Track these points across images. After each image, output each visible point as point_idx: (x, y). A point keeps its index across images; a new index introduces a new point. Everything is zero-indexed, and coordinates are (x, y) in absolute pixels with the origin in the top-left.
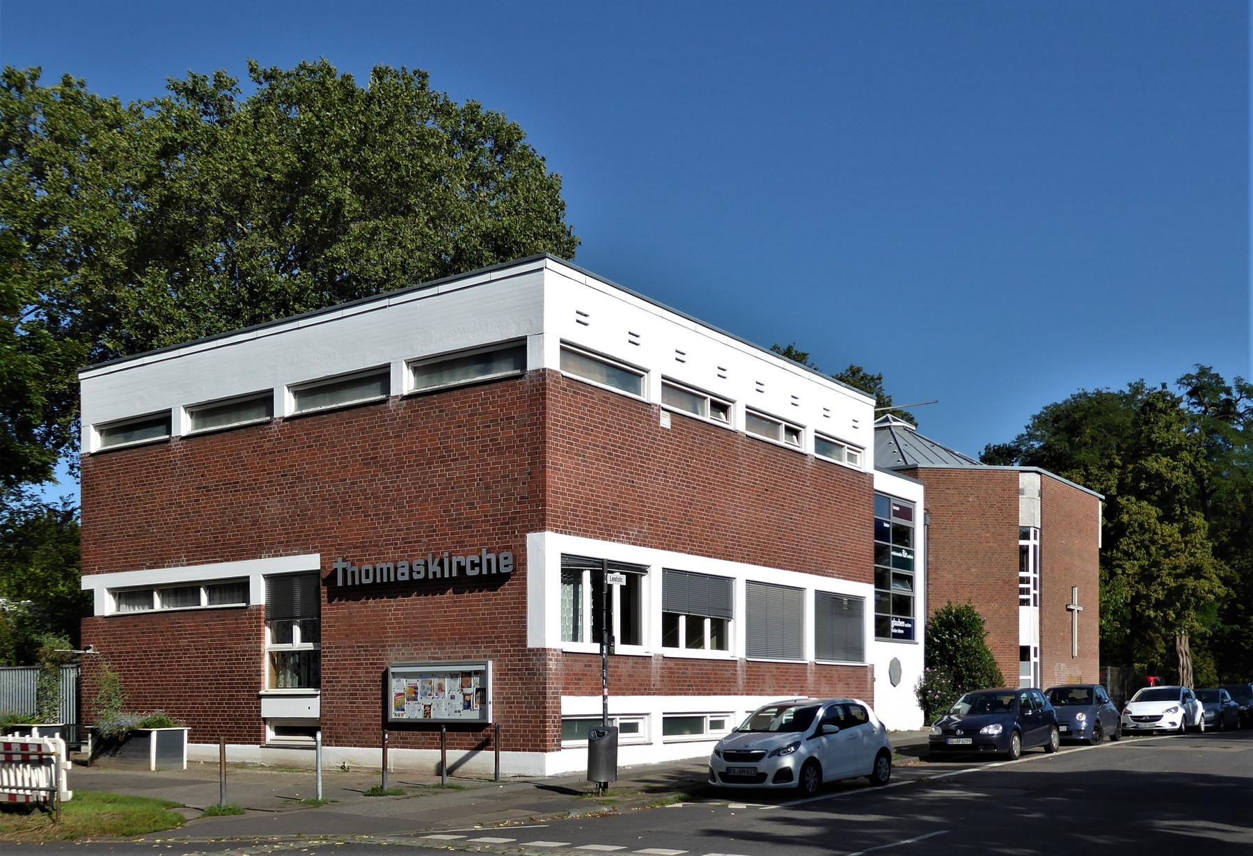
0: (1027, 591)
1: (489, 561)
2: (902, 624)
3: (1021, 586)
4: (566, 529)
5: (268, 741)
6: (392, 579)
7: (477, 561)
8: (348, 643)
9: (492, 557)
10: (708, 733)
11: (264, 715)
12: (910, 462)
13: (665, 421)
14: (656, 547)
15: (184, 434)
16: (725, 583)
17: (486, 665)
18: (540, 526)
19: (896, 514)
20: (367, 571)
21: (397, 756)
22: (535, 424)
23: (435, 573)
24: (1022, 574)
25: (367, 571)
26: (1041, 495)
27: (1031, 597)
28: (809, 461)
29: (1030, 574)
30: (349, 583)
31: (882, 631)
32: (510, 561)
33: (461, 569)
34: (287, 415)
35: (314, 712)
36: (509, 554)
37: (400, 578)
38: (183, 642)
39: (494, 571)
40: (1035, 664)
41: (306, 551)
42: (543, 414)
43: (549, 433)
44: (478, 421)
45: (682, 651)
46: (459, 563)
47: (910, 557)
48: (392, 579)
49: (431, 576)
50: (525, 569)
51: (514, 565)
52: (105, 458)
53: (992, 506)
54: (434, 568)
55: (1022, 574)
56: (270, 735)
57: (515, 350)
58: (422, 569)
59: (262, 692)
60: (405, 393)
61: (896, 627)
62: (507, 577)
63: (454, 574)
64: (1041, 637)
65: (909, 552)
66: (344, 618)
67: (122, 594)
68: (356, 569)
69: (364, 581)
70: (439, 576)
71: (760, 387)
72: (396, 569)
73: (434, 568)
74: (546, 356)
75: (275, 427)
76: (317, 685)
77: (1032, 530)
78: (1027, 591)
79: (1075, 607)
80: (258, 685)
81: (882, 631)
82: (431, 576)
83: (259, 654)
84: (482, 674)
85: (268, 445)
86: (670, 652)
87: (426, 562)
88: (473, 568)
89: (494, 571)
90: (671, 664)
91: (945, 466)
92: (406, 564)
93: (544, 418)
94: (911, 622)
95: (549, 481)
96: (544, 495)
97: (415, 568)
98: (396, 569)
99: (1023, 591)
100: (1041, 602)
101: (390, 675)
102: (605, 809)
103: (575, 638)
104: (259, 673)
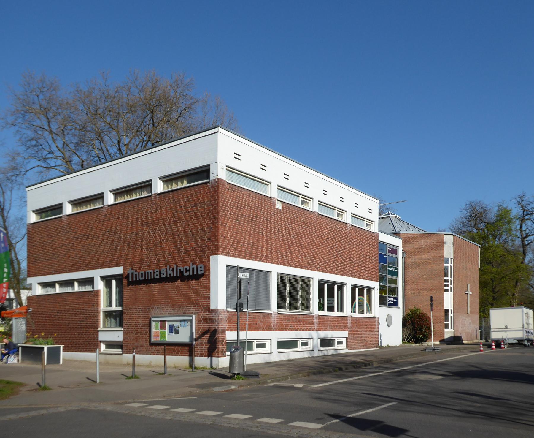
0: (447, 286)
1: (193, 268)
2: (392, 299)
3: (445, 283)
4: (229, 254)
5: (102, 351)
6: (152, 277)
7: (188, 269)
8: (134, 307)
9: (195, 266)
10: (300, 348)
11: (100, 339)
12: (398, 231)
13: (279, 206)
14: (274, 263)
15: (68, 214)
16: (267, 273)
17: (192, 317)
18: (216, 252)
19: (389, 251)
20: (142, 274)
21: (141, 358)
22: (214, 205)
23: (170, 275)
24: (445, 278)
25: (142, 274)
26: (454, 244)
27: (449, 288)
28: (348, 227)
29: (449, 278)
30: (134, 280)
31: (383, 302)
32: (202, 269)
33: (181, 272)
34: (110, 204)
35: (121, 339)
36: (202, 265)
37: (156, 277)
38: (67, 307)
39: (195, 273)
40: (451, 317)
41: (117, 265)
42: (217, 200)
43: (220, 209)
44: (189, 204)
45: (357, 315)
46: (180, 270)
47: (396, 270)
48: (152, 277)
49: (168, 276)
50: (209, 272)
51: (204, 270)
52: (36, 225)
53: (432, 249)
54: (170, 272)
55: (445, 278)
56: (103, 347)
57: (204, 172)
58: (165, 273)
59: (99, 329)
60: (159, 192)
61: (390, 301)
62: (202, 275)
63: (178, 275)
64: (454, 305)
65: (396, 268)
66: (133, 295)
67: (45, 285)
68: (137, 273)
69: (141, 279)
70: (172, 276)
71: (325, 192)
72: (154, 273)
73: (170, 272)
74: (219, 173)
75: (104, 210)
76: (121, 325)
77: (450, 259)
78: (447, 286)
79: (469, 292)
80: (97, 326)
81: (383, 302)
82: (168, 276)
83: (98, 312)
84: (191, 321)
85: (101, 218)
86: (321, 313)
87: (167, 269)
88: (186, 272)
89: (195, 273)
90: (282, 317)
91: (412, 232)
92: (158, 270)
93: (218, 202)
94: (397, 298)
95: (220, 231)
96: (218, 238)
97: (162, 272)
98: (154, 273)
99: (446, 286)
100: (454, 291)
101: (152, 321)
102: (233, 387)
103: (355, 312)
104: (98, 320)
